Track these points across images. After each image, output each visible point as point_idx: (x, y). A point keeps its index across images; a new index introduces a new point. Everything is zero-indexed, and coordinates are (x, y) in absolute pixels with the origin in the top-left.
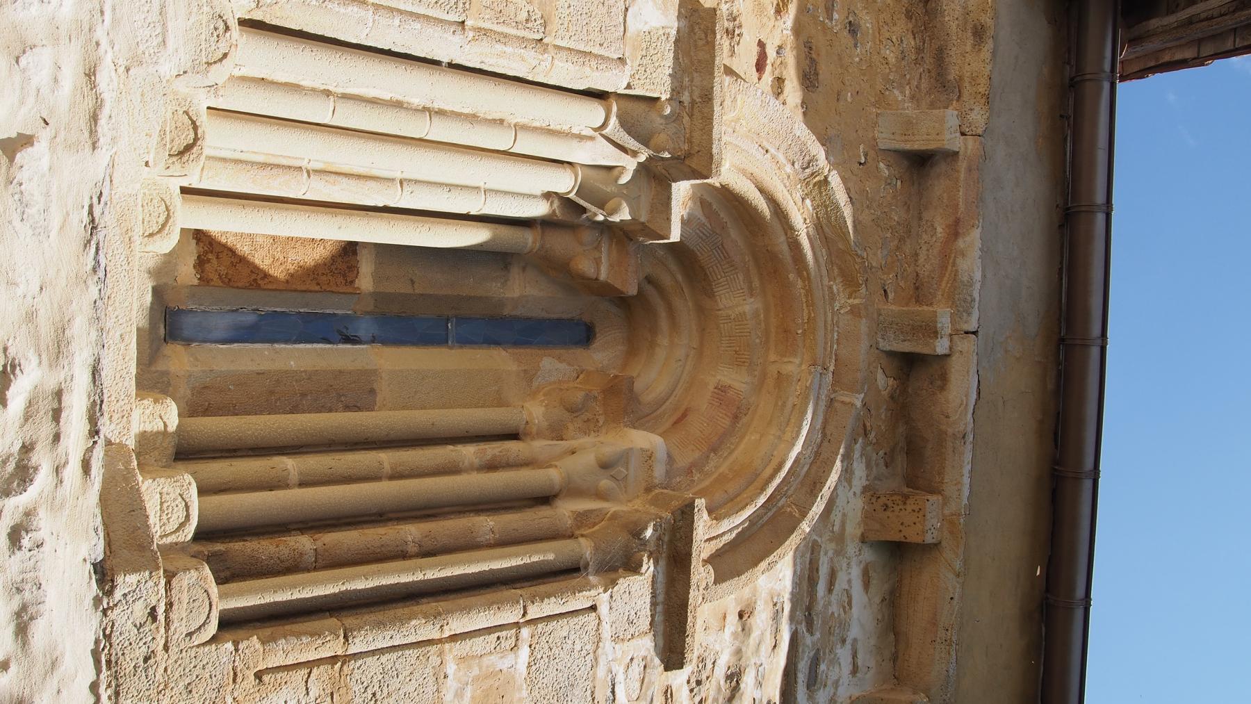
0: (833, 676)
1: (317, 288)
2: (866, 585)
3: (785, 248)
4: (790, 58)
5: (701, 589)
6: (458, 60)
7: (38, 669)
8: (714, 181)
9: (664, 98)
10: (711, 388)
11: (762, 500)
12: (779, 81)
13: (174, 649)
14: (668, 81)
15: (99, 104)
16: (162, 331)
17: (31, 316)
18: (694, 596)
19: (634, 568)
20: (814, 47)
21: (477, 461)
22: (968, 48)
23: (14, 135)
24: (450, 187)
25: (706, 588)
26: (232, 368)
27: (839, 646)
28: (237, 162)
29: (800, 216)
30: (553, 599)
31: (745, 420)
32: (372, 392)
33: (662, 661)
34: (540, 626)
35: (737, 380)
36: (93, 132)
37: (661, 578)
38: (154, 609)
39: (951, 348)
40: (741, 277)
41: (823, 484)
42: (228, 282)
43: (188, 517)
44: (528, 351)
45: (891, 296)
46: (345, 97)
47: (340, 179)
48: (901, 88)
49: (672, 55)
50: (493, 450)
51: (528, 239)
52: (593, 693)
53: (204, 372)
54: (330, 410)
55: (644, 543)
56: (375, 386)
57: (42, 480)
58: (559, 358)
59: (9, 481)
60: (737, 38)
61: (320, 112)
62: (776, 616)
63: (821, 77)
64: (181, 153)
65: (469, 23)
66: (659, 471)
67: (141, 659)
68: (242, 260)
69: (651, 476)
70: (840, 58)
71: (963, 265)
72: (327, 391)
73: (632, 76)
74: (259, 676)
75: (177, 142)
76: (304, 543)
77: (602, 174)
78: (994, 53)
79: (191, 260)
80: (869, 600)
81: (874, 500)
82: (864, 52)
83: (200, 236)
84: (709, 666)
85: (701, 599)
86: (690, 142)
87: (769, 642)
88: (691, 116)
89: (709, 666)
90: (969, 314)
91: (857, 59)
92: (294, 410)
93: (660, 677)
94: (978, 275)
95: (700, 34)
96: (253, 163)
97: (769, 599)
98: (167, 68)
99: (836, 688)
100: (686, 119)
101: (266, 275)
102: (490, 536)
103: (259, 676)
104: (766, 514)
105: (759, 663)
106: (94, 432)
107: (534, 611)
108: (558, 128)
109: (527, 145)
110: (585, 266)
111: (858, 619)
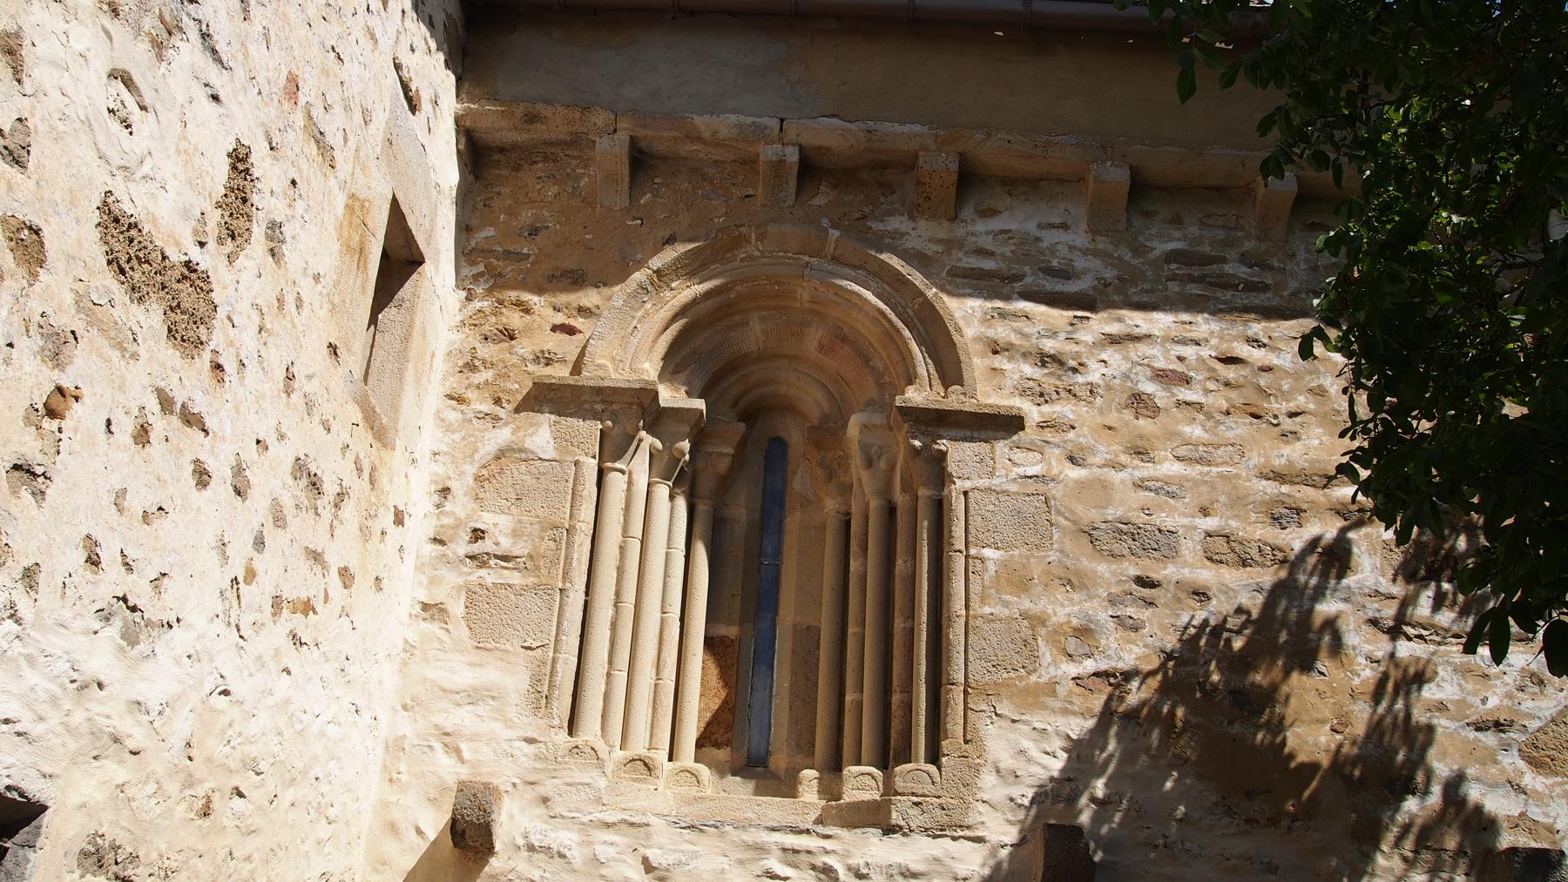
0: (1063, 251)
1: (735, 667)
2: (991, 213)
3: (710, 303)
4: (563, 298)
5: (964, 400)
6: (583, 588)
7: (939, 868)
8: (656, 379)
9: (600, 427)
10: (821, 356)
11: (907, 333)
12: (583, 311)
13: (940, 793)
14: (588, 422)
15: (624, 821)
16: (760, 769)
17: (741, 862)
18: (969, 406)
19: (943, 455)
20: (552, 273)
21: (860, 560)
22: (544, 127)
23: (643, 867)
24: (666, 575)
25: (964, 394)
26: (786, 726)
27: (1041, 244)
28: (652, 727)
29: (686, 291)
30: (953, 528)
31: (846, 330)
32: (808, 628)
33: (1015, 433)
34: (970, 539)
35: (815, 336)
36: (640, 826)
37: (953, 433)
38: (914, 804)
39: (794, 145)
40: (733, 334)
41: (899, 273)
42: (730, 728)
43: (868, 774)
44: (787, 498)
45: (751, 192)
46: (610, 662)
47: (662, 658)
48: (578, 178)
49: (569, 419)
50: (854, 547)
51: (703, 508)
52: (1028, 495)
53: (787, 745)
54: (818, 660)
55: (925, 447)
56: (804, 626)
57: (831, 861)
58: (795, 473)
59: (831, 878)
60: (552, 356)
61: (621, 677)
62: (1003, 315)
63: (575, 268)
64: (649, 769)
65: (560, 585)
66: (878, 419)
67: (943, 812)
68: (715, 716)
69: (881, 426)
70: (558, 246)
71: (724, 133)
72: (806, 662)
73: (587, 454)
74: (966, 742)
75: (642, 771)
76: (896, 698)
77: (654, 460)
78: (548, 102)
79: (715, 751)
80: (1007, 209)
81: (920, 209)
82: (550, 219)
83: (700, 744)
84: (1031, 384)
85: (972, 400)
86: (632, 404)
87: (1021, 324)
88: (612, 403)
89: (1031, 384)
90: (766, 128)
91: (558, 226)
92: (816, 685)
93: (1029, 434)
94: (733, 118)
95: (552, 395)
96: (653, 716)
97: (987, 323)
98: (602, 783)
99: (1076, 248)
100: (615, 407)
101: (725, 702)
102: (909, 563)
103: (966, 742)
104: (918, 329)
105: (1037, 335)
106: (808, 832)
107: (959, 544)
108: (623, 501)
109: (637, 528)
110: (723, 465)
111: (1021, 223)
